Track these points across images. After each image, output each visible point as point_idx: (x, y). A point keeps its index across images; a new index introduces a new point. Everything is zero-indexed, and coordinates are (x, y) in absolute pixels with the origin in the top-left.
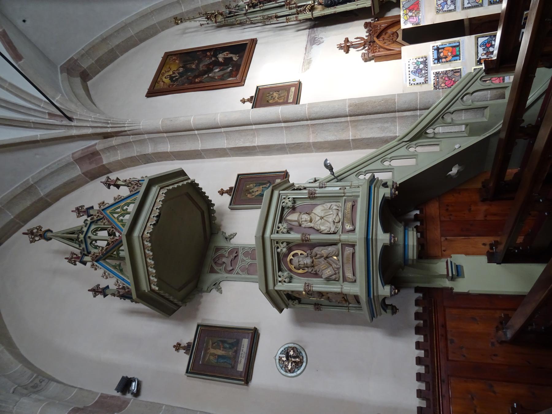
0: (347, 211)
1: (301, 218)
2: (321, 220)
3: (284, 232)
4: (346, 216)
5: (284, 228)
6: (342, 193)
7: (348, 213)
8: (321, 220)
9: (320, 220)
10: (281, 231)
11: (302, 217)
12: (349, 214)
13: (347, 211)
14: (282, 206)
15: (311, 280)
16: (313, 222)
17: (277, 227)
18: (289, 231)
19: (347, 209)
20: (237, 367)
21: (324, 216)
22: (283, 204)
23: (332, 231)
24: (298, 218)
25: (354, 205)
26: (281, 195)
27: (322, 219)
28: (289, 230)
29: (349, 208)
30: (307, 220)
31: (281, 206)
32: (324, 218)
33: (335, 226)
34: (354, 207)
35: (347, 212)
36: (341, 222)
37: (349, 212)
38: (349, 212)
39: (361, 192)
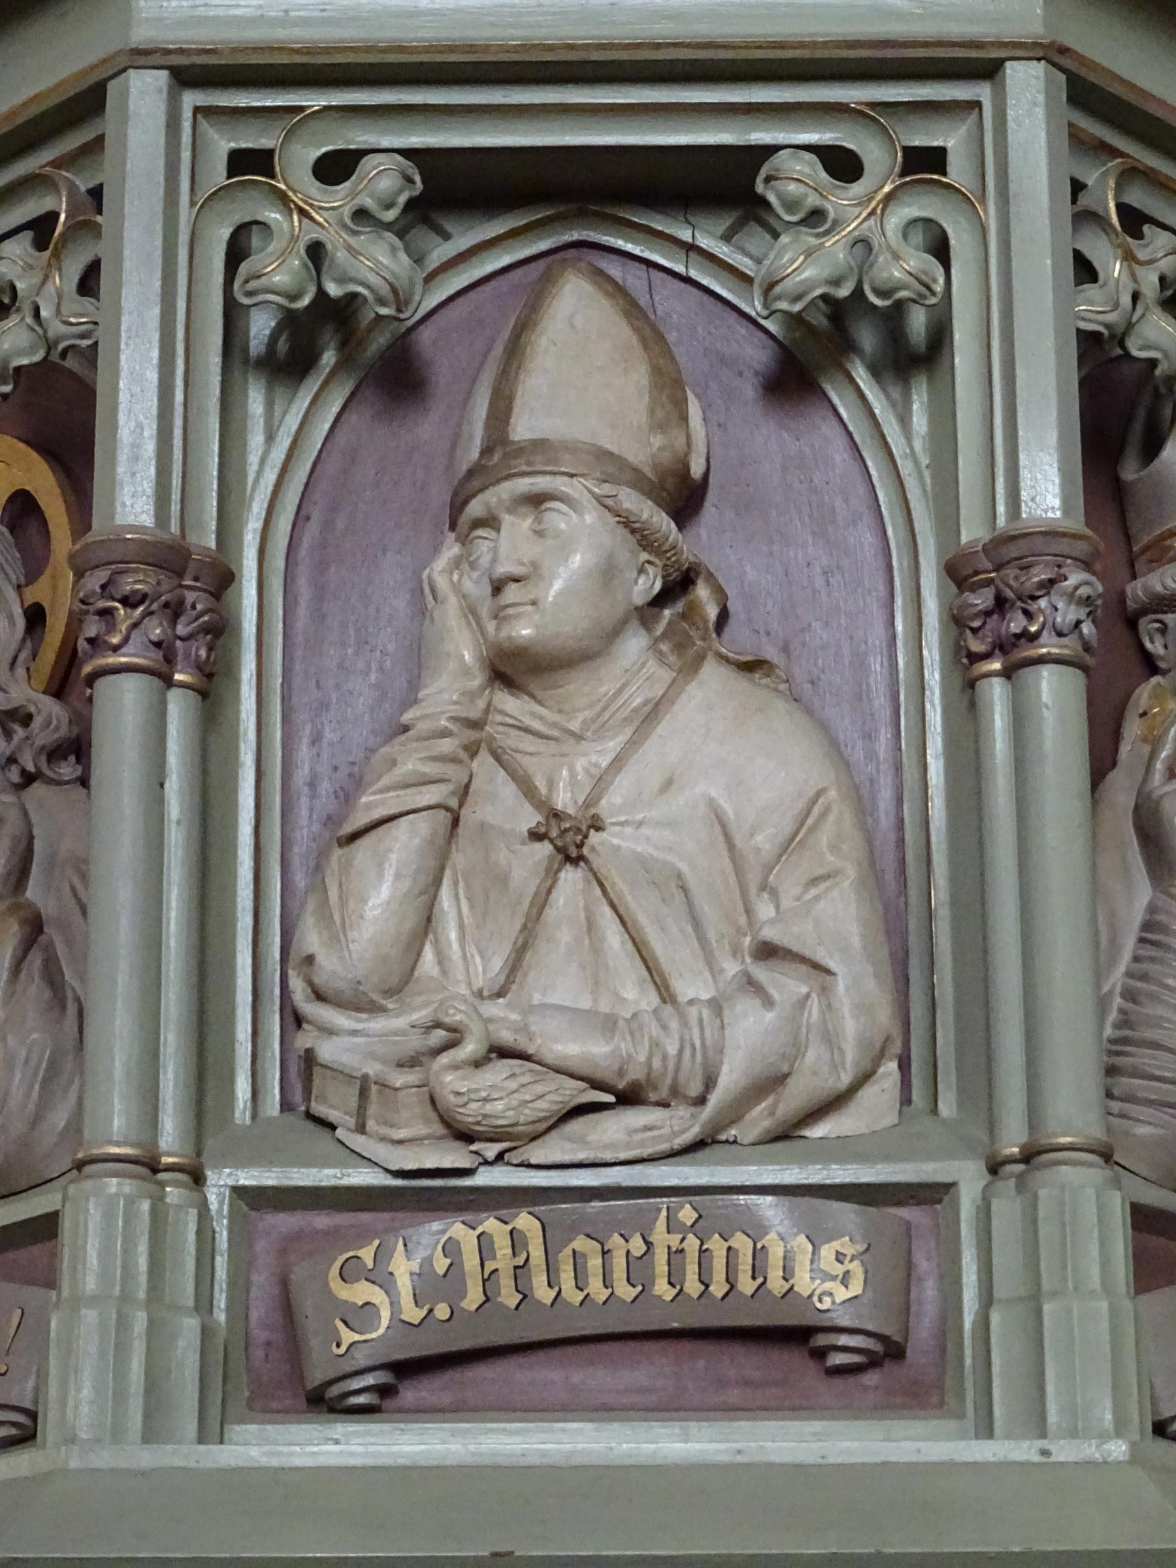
0: (676, 1255)
1: (537, 500)
2: (536, 836)
3: (244, 268)
4: (580, 1243)
5: (316, 252)
6: (1034, 1116)
7: (638, 1270)
8: (536, 836)
9: (531, 818)
10: (274, 216)
11: (558, 519)
12: (627, 1292)
13: (676, 1255)
14: (773, 149)
15: (722, 1200)
16: (508, 703)
17: (358, 137)
18: (349, 343)
19: (717, 1246)
20: (65, 501)
21: (620, 885)
22: (809, 168)
23: (330, 1032)
24: (540, 445)
25: (820, 1354)
26: (982, 92)
27: (545, 848)
28: (380, 340)
29: (746, 1285)
30: (512, 593)
31: (760, 136)
32: (571, 877)
33: (372, 1069)
34: (792, 1360)
35: (661, 1237)
36: (453, 1156)
37: (662, 1288)
38: (662, 1288)
39: (1025, 1451)
